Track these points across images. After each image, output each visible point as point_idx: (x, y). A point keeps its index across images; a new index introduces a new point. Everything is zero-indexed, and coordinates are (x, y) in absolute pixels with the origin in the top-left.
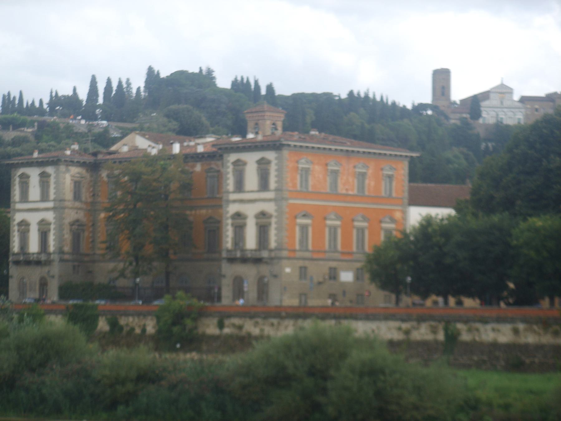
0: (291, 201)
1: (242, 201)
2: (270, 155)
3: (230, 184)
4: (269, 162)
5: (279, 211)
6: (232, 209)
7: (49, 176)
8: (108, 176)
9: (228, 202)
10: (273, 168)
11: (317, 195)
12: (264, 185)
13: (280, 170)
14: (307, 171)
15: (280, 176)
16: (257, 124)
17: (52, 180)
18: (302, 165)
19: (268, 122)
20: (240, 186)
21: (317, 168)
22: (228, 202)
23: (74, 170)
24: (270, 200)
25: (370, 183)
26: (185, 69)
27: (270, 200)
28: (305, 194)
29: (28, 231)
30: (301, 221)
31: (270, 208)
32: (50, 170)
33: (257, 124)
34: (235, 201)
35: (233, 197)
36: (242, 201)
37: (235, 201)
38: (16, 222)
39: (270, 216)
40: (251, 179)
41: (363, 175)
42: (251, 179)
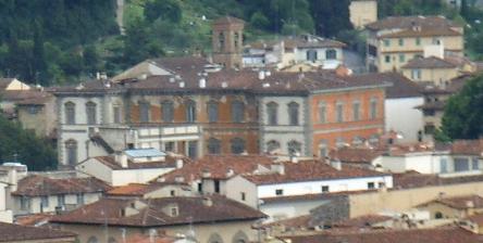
0: (318, 132)
1: (275, 132)
2: (299, 100)
3: (265, 118)
4: (297, 105)
5: (307, 141)
6: (268, 138)
7: (95, 105)
8: (139, 102)
9: (264, 132)
10: (301, 110)
11: (331, 125)
12: (294, 121)
13: (306, 111)
14: (323, 109)
15: (307, 117)
16: (221, 34)
17: (98, 109)
18: (320, 106)
19: (232, 33)
20: (273, 121)
21: (329, 106)
22: (264, 132)
23: (114, 99)
24: (299, 133)
25: (361, 110)
26: (414, 169)
27: (299, 133)
28: (322, 126)
29: (76, 148)
30: (321, 146)
31: (300, 138)
32: (95, 100)
33: (221, 34)
34: (270, 132)
35: (267, 129)
36: (275, 132)
37: (270, 132)
38: (63, 141)
39: (300, 144)
40: (283, 116)
41: (357, 105)
42: (283, 116)
